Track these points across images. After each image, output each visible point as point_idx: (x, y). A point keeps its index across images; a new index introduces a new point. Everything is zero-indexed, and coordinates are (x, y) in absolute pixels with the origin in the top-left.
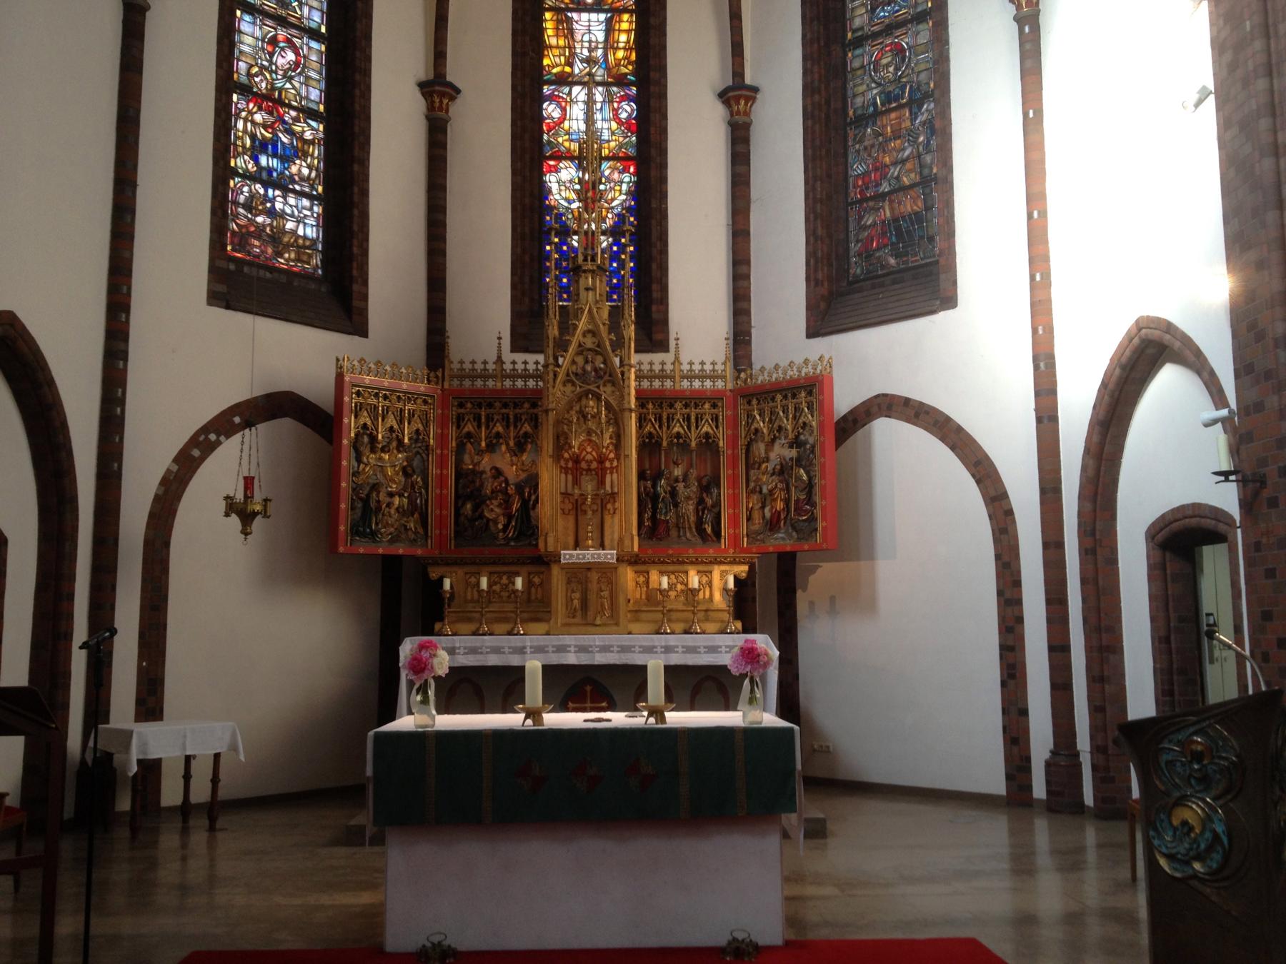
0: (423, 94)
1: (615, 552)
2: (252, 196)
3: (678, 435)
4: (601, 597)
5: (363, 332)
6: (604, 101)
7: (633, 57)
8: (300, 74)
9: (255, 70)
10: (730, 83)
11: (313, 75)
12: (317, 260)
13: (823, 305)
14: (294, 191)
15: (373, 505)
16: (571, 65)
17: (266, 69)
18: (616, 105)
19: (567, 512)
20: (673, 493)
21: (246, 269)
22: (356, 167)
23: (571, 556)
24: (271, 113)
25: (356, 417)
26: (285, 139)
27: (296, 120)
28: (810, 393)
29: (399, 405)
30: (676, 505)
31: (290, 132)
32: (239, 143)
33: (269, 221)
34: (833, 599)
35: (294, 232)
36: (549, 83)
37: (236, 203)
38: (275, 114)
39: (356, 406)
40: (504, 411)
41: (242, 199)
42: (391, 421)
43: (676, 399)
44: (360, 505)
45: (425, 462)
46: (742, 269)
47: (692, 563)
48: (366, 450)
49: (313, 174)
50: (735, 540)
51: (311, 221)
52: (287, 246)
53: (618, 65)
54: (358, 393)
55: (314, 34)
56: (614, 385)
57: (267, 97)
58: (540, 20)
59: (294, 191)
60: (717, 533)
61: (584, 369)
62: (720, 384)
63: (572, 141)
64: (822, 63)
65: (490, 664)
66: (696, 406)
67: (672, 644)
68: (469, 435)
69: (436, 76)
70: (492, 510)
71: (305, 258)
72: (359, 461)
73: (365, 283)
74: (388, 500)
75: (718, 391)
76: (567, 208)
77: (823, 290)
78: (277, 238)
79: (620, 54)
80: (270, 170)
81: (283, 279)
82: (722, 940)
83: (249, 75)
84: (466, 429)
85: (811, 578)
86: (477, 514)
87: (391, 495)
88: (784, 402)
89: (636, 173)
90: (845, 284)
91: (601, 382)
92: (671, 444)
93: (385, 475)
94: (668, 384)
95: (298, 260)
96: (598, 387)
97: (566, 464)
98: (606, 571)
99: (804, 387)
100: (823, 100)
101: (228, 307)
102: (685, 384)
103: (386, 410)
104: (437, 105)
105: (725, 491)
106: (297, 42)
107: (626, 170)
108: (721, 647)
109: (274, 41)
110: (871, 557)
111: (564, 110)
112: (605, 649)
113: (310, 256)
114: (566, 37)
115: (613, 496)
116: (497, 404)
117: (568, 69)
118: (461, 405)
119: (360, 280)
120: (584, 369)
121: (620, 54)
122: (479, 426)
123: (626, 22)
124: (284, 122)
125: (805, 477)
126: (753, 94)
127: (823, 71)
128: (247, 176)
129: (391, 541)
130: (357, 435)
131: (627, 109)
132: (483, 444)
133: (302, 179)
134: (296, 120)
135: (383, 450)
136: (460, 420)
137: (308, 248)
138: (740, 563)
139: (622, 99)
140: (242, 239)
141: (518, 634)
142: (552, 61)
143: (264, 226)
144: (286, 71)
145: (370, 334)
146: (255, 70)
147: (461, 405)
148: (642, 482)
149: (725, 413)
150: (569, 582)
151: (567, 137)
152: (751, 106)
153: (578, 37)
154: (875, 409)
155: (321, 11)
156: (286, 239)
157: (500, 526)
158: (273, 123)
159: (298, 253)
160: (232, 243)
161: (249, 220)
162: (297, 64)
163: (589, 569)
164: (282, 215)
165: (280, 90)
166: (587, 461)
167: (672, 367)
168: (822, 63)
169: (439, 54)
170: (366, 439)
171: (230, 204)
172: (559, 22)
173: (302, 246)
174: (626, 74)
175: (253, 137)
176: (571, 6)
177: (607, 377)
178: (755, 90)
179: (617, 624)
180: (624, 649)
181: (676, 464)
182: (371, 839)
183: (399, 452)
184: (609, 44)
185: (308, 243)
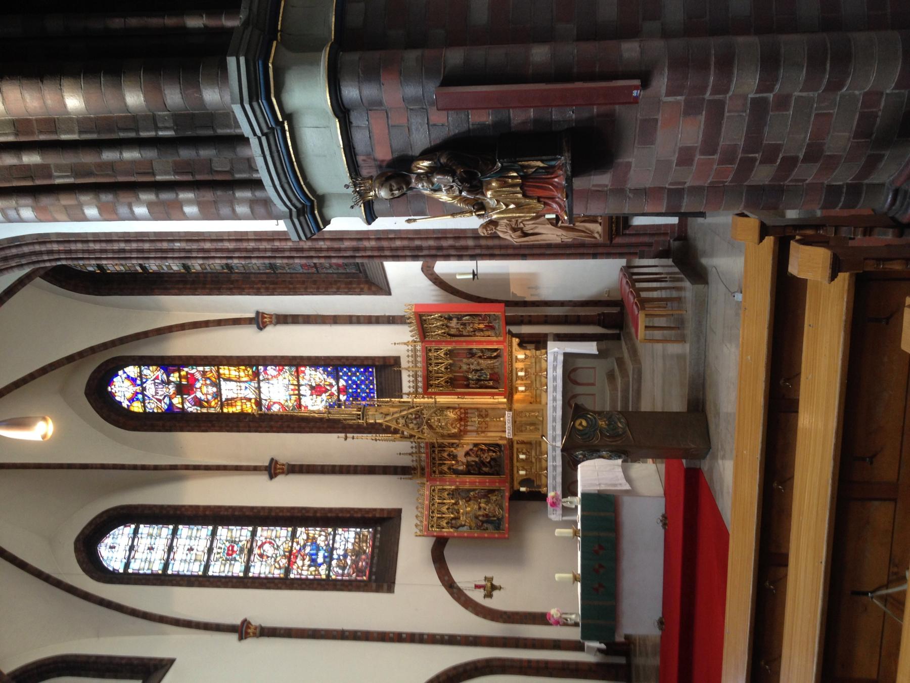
0: (276, 477)
1: (507, 412)
2: (338, 566)
3: (446, 368)
4: (529, 416)
5: (399, 512)
6: (268, 383)
7: (243, 367)
8: (275, 541)
9: (277, 566)
10: (255, 326)
11: (274, 533)
12: (365, 531)
13: (374, 289)
14: (333, 544)
15: (485, 519)
16: (250, 400)
17: (275, 560)
18: (270, 377)
19: (486, 426)
20: (476, 371)
21: (374, 570)
22: (318, 515)
23: (509, 433)
24: (296, 557)
25: (443, 528)
26: (308, 549)
27: (298, 543)
28: (424, 315)
29: (436, 505)
30: (482, 370)
31: (304, 546)
32: (313, 573)
33: (349, 557)
34: (529, 288)
35: (353, 544)
36: (261, 410)
37: (343, 575)
38: (297, 554)
39: (438, 528)
40: (436, 452)
41: (340, 572)
42: (444, 509)
43: (428, 370)
44: (485, 525)
45: (463, 490)
46: (354, 319)
47: (512, 366)
48: (459, 522)
49: (323, 533)
50: (498, 342)
51: (346, 534)
52: (361, 548)
53: (248, 375)
54: (432, 526)
55: (254, 534)
56: (423, 410)
57: (289, 558)
58: (228, 414)
59: (333, 544)
60: (496, 350)
61: (416, 424)
62: (419, 348)
63: (290, 399)
64: (244, 286)
65: (561, 481)
66: (430, 359)
67: (552, 398)
68: (449, 469)
69: (266, 470)
70: (486, 457)
71: (365, 538)
72: (464, 525)
73: (375, 510)
74: (482, 509)
75: (422, 349)
76: (326, 401)
77: (366, 287)
78: (357, 553)
79: (242, 374)
80: (325, 557)
81: (376, 551)
82: (661, 532)
83: (280, 568)
84: (446, 470)
85: (518, 295)
86: (488, 465)
87: (480, 508)
88: (433, 351)
89: (305, 366)
90: (361, 274)
91: (422, 416)
92: (451, 372)
93: (471, 511)
94: (420, 373)
95: (366, 542)
96: (424, 418)
97: (463, 426)
98: (516, 415)
99: (427, 353)
100: (263, 286)
101: (394, 583)
102: (419, 365)
103: (439, 512)
104: (281, 471)
105: (474, 347)
106: (259, 543)
107: (303, 372)
108: (553, 375)
109: (261, 556)
110: (508, 274)
111: (275, 403)
112: (554, 429)
113: (363, 535)
114: (236, 402)
115: (479, 434)
116: (433, 455)
117: (253, 401)
118: (434, 472)
119: (374, 513)
120: (416, 424)
121: (242, 374)
122: (445, 464)
123: (224, 370)
124: (300, 549)
125: (467, 317)
126: (260, 314)
127: (248, 286)
128: (329, 569)
129: (502, 509)
130: (452, 527)
131: (271, 370)
132: (454, 462)
133: (326, 540)
134: (298, 543)
135: (458, 513)
136: (441, 473)
137: (360, 537)
138: (511, 342)
139: (266, 373)
140: (360, 571)
141: (547, 474)
142: (249, 408)
143: (352, 560)
144: (275, 549)
145: (398, 507)
146: (277, 566)
147: (434, 472)
148: (471, 386)
149: (434, 346)
150: (522, 431)
151: (289, 401)
152: (267, 314)
153: (235, 396)
154: (430, 272)
155: (241, 530)
156: (357, 548)
157: (494, 454)
158: (301, 555)
159: (363, 542)
160: (362, 576)
161: (350, 567)
162: (270, 543)
163: (515, 422)
164: (346, 550)
165: (284, 552)
166: (460, 426)
167: (411, 372)
168: (244, 286)
169: (256, 469)
170: (453, 522)
171: (344, 578)
172: (228, 405)
173: (359, 539)
174: (253, 371)
175: (309, 566)
176: (219, 399)
177: (419, 413)
178: (258, 313)
179: (543, 410)
180: (554, 420)
181: (460, 368)
182: (704, 190)
183: (459, 504)
184: (238, 380)
185: (357, 537)
